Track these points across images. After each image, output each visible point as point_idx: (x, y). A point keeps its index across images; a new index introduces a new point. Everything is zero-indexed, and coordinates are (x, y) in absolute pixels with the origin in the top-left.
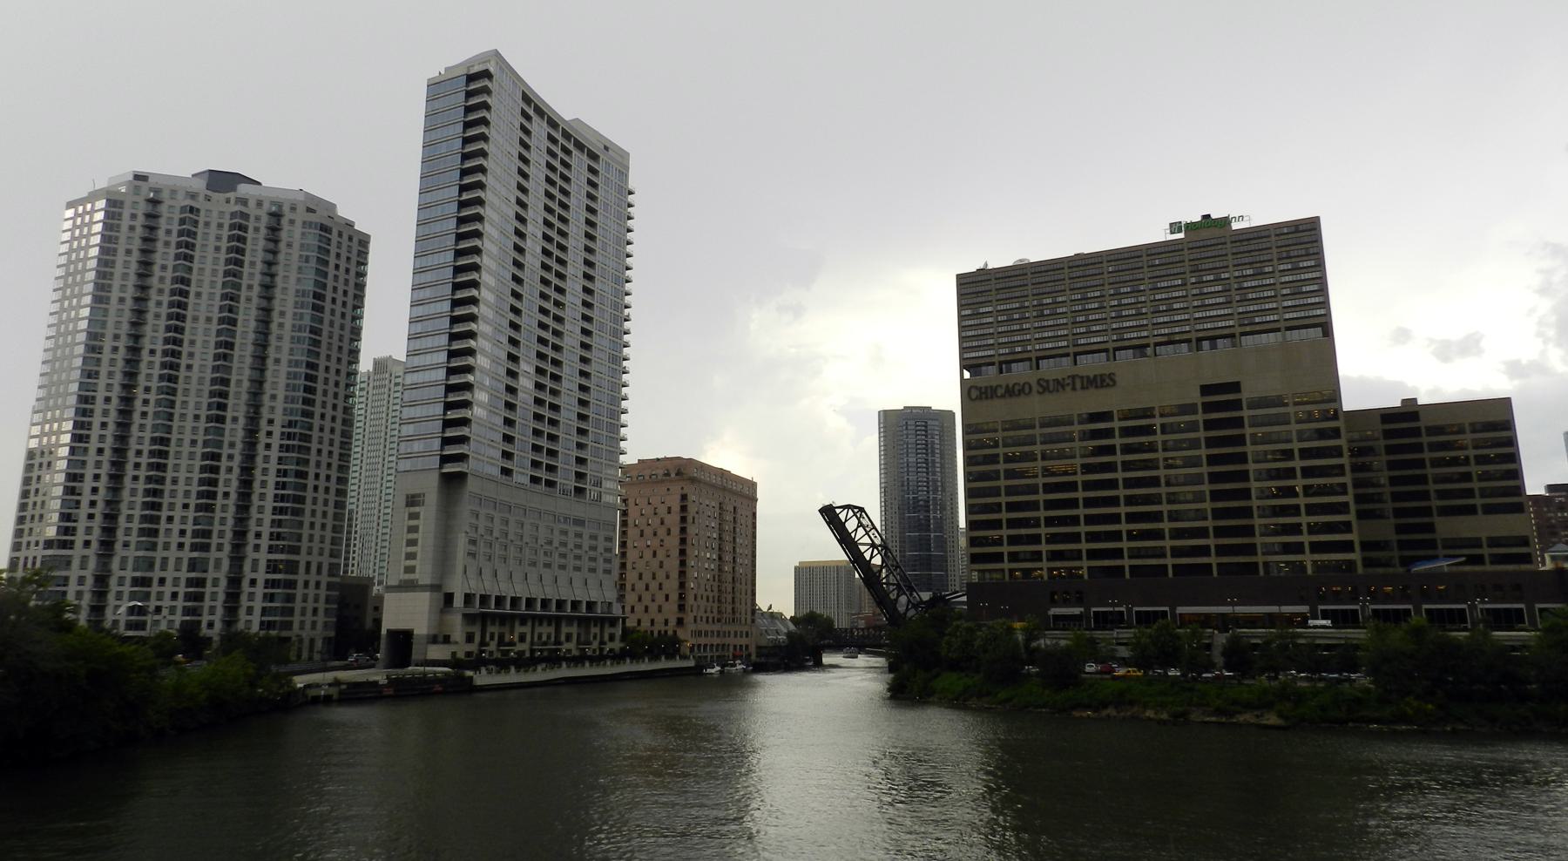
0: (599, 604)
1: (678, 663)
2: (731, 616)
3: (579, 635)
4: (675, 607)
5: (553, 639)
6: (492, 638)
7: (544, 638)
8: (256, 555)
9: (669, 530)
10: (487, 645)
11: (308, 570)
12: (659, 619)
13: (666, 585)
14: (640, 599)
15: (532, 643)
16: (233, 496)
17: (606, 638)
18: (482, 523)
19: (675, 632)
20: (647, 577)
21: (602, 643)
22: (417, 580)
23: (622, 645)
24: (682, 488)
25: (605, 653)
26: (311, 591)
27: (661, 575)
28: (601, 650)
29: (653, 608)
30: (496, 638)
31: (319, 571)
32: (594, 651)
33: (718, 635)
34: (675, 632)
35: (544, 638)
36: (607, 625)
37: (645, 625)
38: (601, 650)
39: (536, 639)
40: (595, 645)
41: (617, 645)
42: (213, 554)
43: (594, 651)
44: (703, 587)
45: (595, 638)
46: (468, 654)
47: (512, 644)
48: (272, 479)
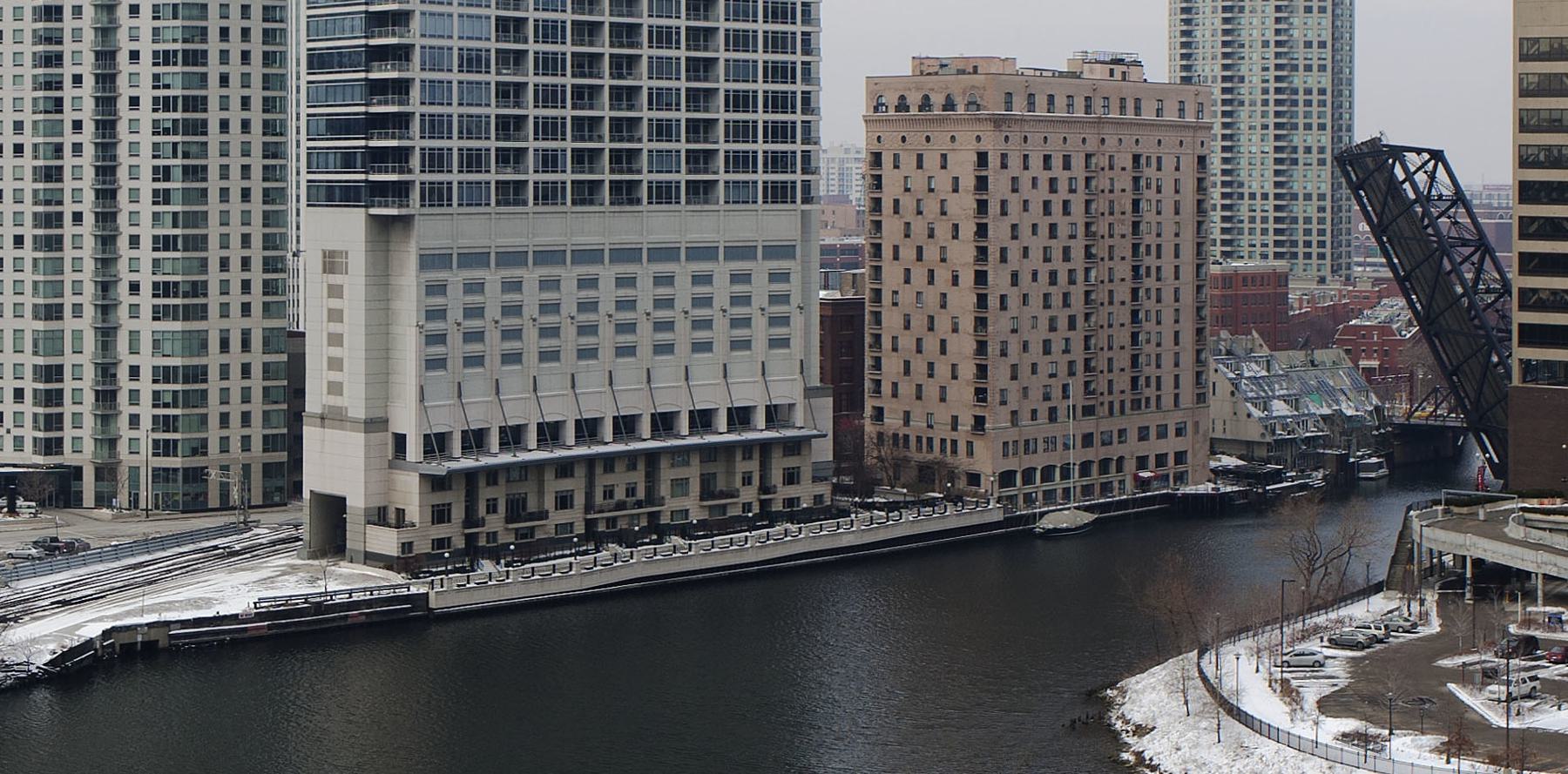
2: (1128, 397)
4: (969, 393)
7: (620, 494)
8: (134, 325)
9: (956, 227)
10: (482, 523)
11: (225, 345)
12: (942, 415)
13: (953, 342)
14: (907, 371)
15: (589, 507)
16: (89, 219)
18: (455, 301)
20: (918, 322)
21: (765, 488)
24: (978, 139)
26: (235, 383)
28: (764, 504)
30: (502, 508)
31: (246, 345)
39: (599, 498)
42: (69, 323)
45: (747, 480)
46: (440, 543)
47: (543, 515)
48: (146, 185)
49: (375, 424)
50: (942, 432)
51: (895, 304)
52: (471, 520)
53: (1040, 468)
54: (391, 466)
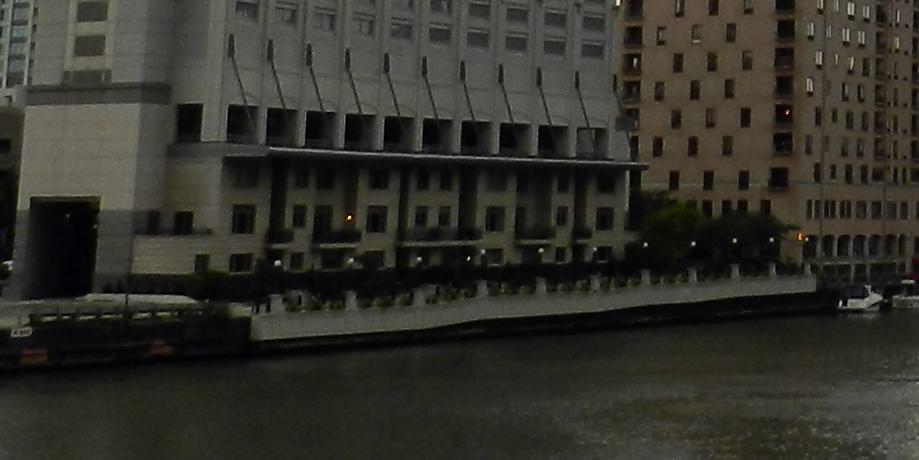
0: (573, 134)
1: (772, 285)
3: (520, 213)
4: (766, 143)
5: (454, 222)
6: (299, 220)
7: (433, 221)
12: (726, 171)
15: (401, 234)
17: (591, 219)
19: (766, 205)
20: (694, 64)
21: (580, 232)
22: (108, 73)
23: (631, 238)
25: (588, 258)
27: (730, 60)
28: (578, 250)
29: (710, 142)
30: (310, 220)
32: (560, 253)
33: (876, 214)
34: (766, 205)
35: (433, 221)
36: (591, 189)
37: (691, 186)
38: (578, 250)
39: (411, 223)
40: (562, 238)
41: (617, 239)
43: (560, 253)
44: (836, 91)
45: (562, 218)
46: (239, 261)
49: (153, 92)
50: (725, 191)
51: (661, 43)
52: (275, 234)
53: (837, 237)
54: (171, 153)
